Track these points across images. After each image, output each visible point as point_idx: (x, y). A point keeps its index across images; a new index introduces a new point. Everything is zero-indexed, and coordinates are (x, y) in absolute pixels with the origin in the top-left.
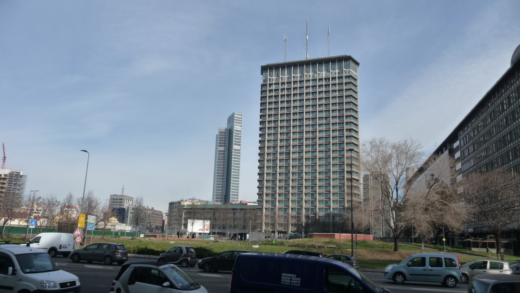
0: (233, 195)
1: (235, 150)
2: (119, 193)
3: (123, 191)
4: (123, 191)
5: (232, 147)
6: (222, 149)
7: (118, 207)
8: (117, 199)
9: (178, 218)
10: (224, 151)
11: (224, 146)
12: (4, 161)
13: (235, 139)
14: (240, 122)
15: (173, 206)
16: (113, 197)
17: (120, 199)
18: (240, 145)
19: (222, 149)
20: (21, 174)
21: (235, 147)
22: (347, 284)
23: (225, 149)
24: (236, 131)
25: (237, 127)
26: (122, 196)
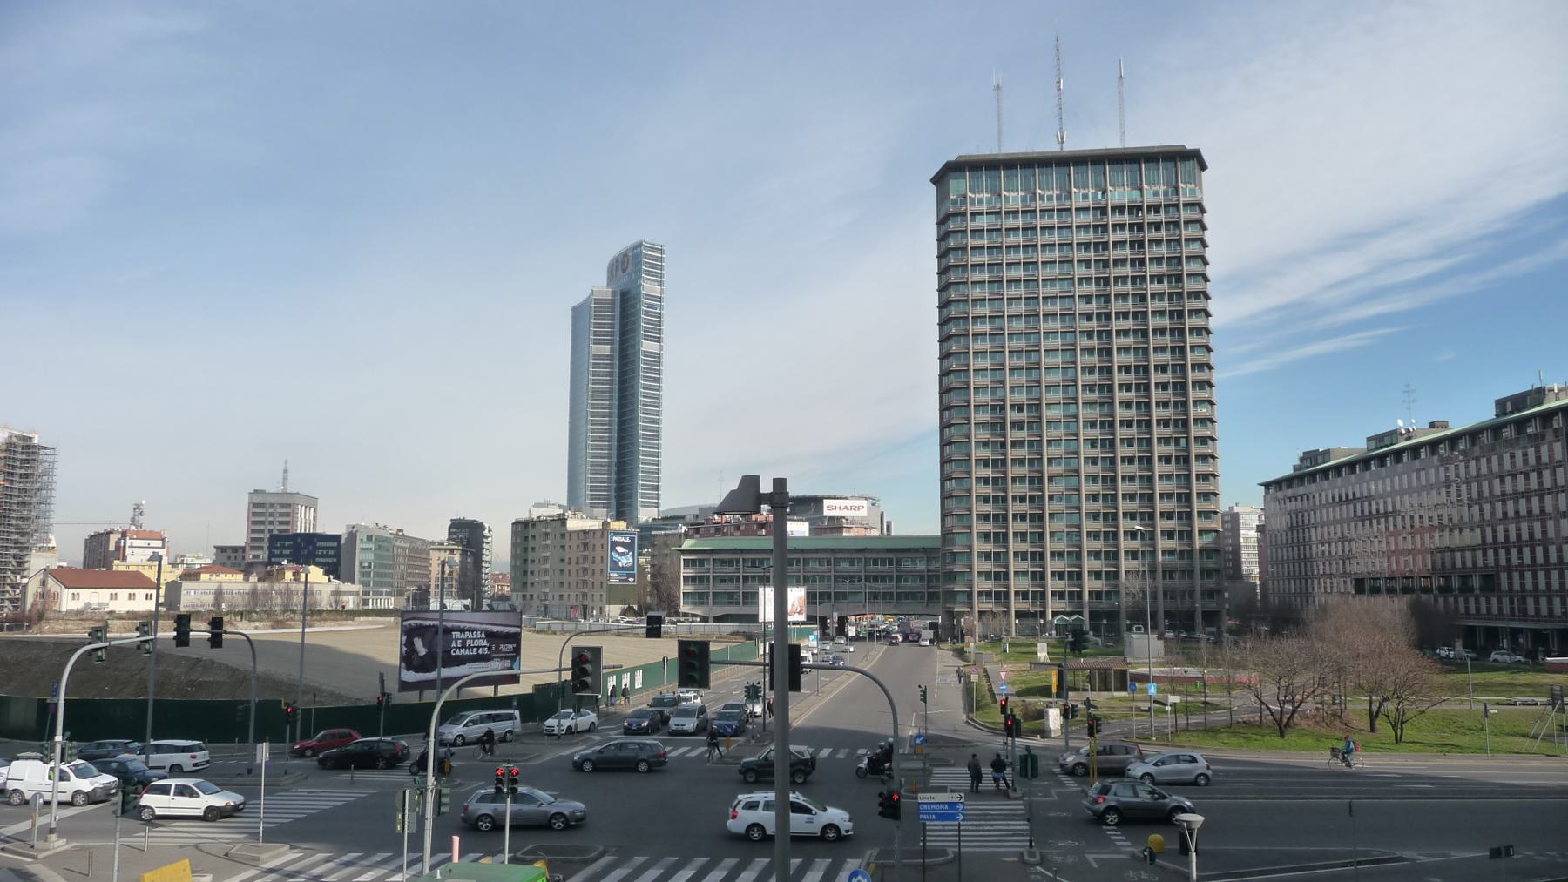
0: (644, 487)
1: (647, 354)
2: (272, 486)
3: (285, 479)
4: (285, 479)
5: (636, 346)
6: (605, 350)
7: (276, 528)
8: (272, 505)
9: (1443, 450)
10: (611, 358)
11: (611, 342)
12: (286, 471)
13: (646, 362)
14: (657, 271)
15: (531, 532)
16: (258, 500)
17: (282, 506)
18: (659, 340)
19: (605, 350)
20: (36, 441)
21: (647, 346)
22: (508, 462)
23: (612, 350)
24: (649, 297)
25: (648, 287)
26: (284, 493)
